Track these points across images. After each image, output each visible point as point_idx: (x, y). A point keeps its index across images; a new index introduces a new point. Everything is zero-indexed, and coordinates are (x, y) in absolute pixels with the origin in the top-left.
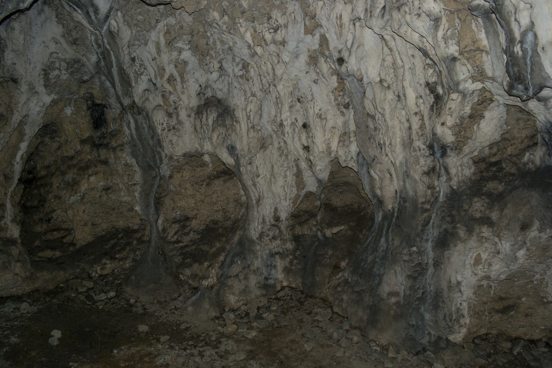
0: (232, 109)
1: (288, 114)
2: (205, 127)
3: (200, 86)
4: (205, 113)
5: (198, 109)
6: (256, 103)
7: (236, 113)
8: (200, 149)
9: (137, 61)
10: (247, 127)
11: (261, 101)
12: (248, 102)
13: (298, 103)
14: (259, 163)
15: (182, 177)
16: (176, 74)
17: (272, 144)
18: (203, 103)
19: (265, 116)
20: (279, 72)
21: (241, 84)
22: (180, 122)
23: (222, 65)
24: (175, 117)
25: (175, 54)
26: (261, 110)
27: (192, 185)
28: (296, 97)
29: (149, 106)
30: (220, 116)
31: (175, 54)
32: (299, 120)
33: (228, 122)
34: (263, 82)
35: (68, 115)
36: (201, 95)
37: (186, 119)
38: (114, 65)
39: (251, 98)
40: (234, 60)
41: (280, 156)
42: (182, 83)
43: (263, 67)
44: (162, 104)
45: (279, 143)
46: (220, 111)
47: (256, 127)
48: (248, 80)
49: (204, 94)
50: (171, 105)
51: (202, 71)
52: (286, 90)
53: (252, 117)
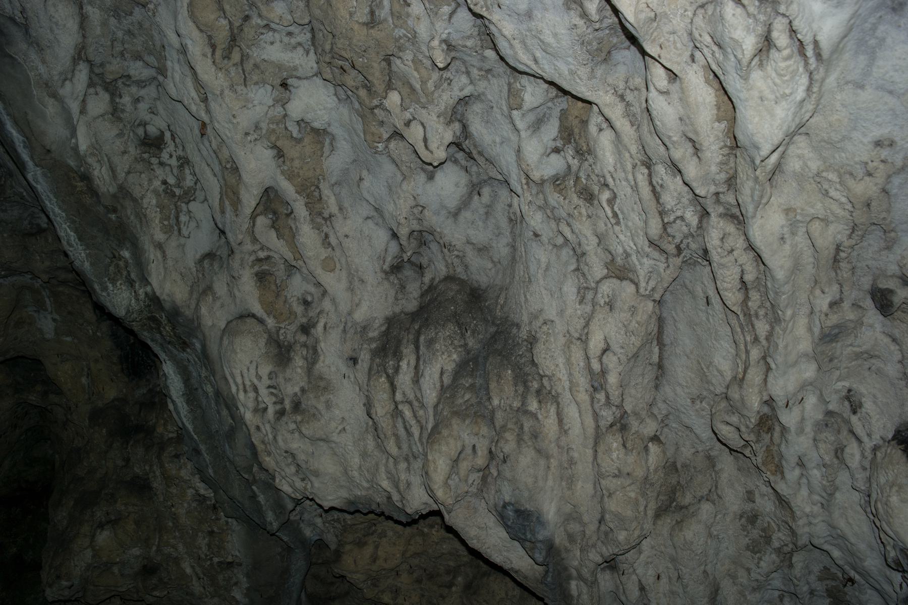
0: (524, 334)
1: (809, 371)
2: (408, 413)
3: (395, 236)
4: (408, 351)
5: (386, 334)
6: (633, 310)
7: (541, 354)
8: (396, 497)
9: (171, 147)
10: (590, 422)
11: (659, 303)
12: (594, 304)
13: (873, 316)
14: (651, 572)
15: (374, 559)
16: (287, 188)
17: (713, 496)
18: (412, 305)
19: (681, 370)
20: (764, 124)
21: (558, 220)
22: (318, 384)
23: (465, 127)
24: (299, 362)
25: (262, 97)
26: (661, 344)
27: (419, 581)
28: (866, 282)
29: (213, 317)
30: (469, 365)
31: (262, 97)
32: (868, 405)
33: (503, 395)
34: (668, 200)
35: (47, 336)
36: (408, 272)
37: (344, 369)
38: (25, 156)
39: (606, 288)
40: (514, 100)
41: (755, 548)
42: (318, 228)
43: (659, 104)
44: (257, 309)
45: (750, 496)
46: (471, 342)
47: (634, 425)
48: (589, 197)
49: (420, 269)
50: (292, 313)
51: (389, 168)
52: (801, 239)
53: (612, 379)
